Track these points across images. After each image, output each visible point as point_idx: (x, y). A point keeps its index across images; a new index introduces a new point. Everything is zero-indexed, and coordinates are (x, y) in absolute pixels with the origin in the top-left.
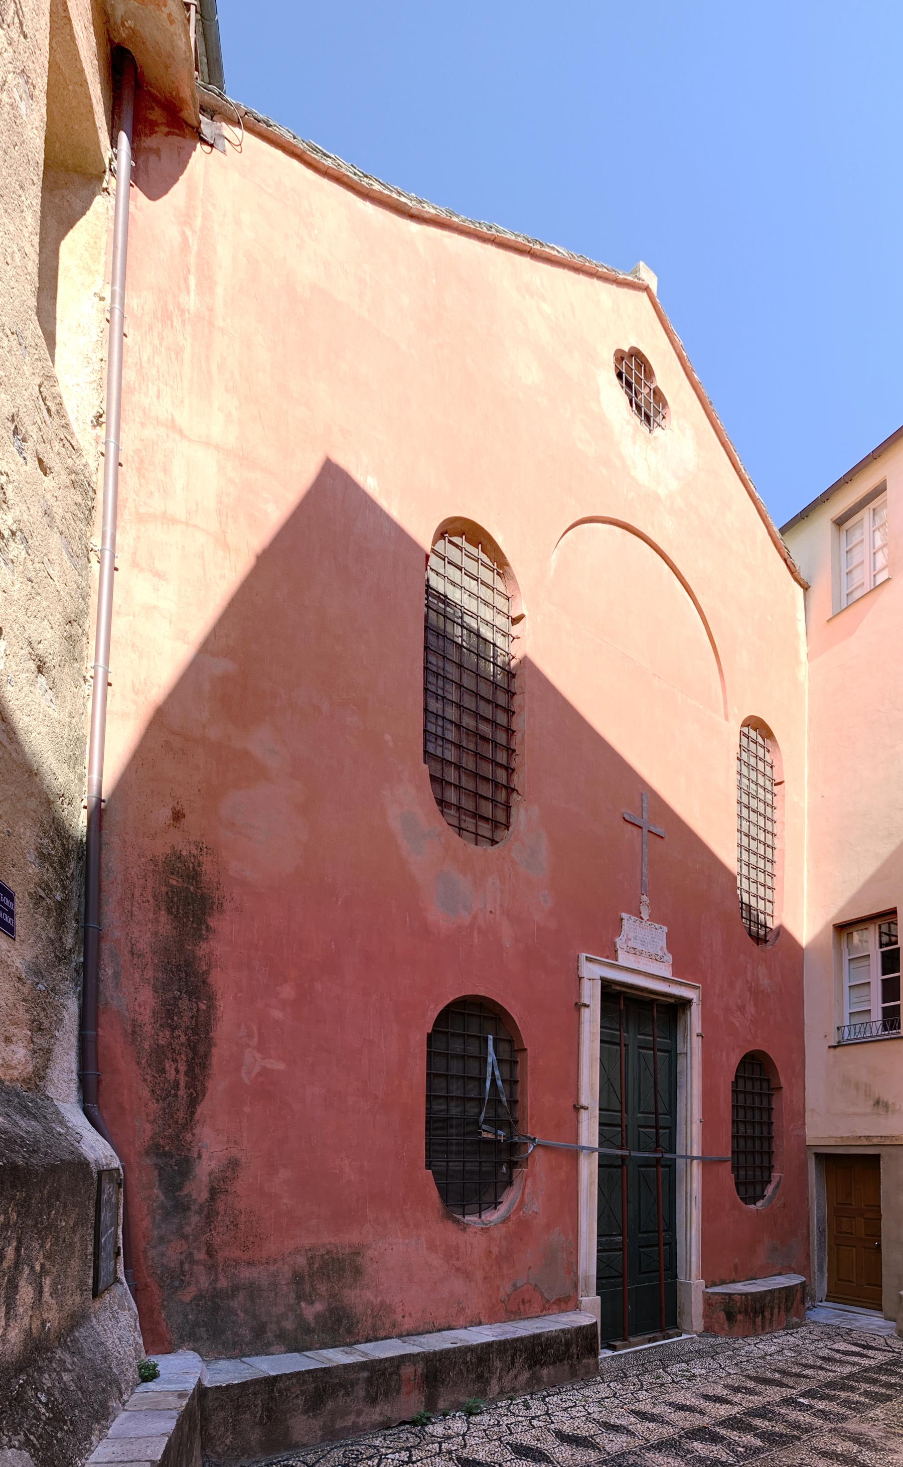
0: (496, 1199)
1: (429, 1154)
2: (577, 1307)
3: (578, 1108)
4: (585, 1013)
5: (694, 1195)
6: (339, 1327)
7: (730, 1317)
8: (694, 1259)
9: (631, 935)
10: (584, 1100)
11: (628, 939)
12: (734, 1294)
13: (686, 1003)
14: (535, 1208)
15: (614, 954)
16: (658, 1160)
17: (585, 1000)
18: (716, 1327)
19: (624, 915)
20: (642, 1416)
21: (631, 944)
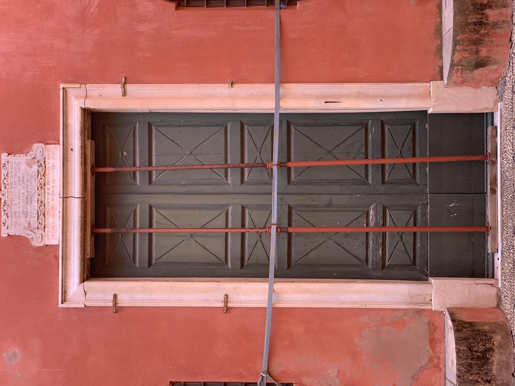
4: (124, 301)
6: (471, 234)
7: (481, 64)
9: (23, 221)
12: (452, 60)
14: (333, 373)
15: (49, 250)
16: (280, 230)
18: (493, 76)
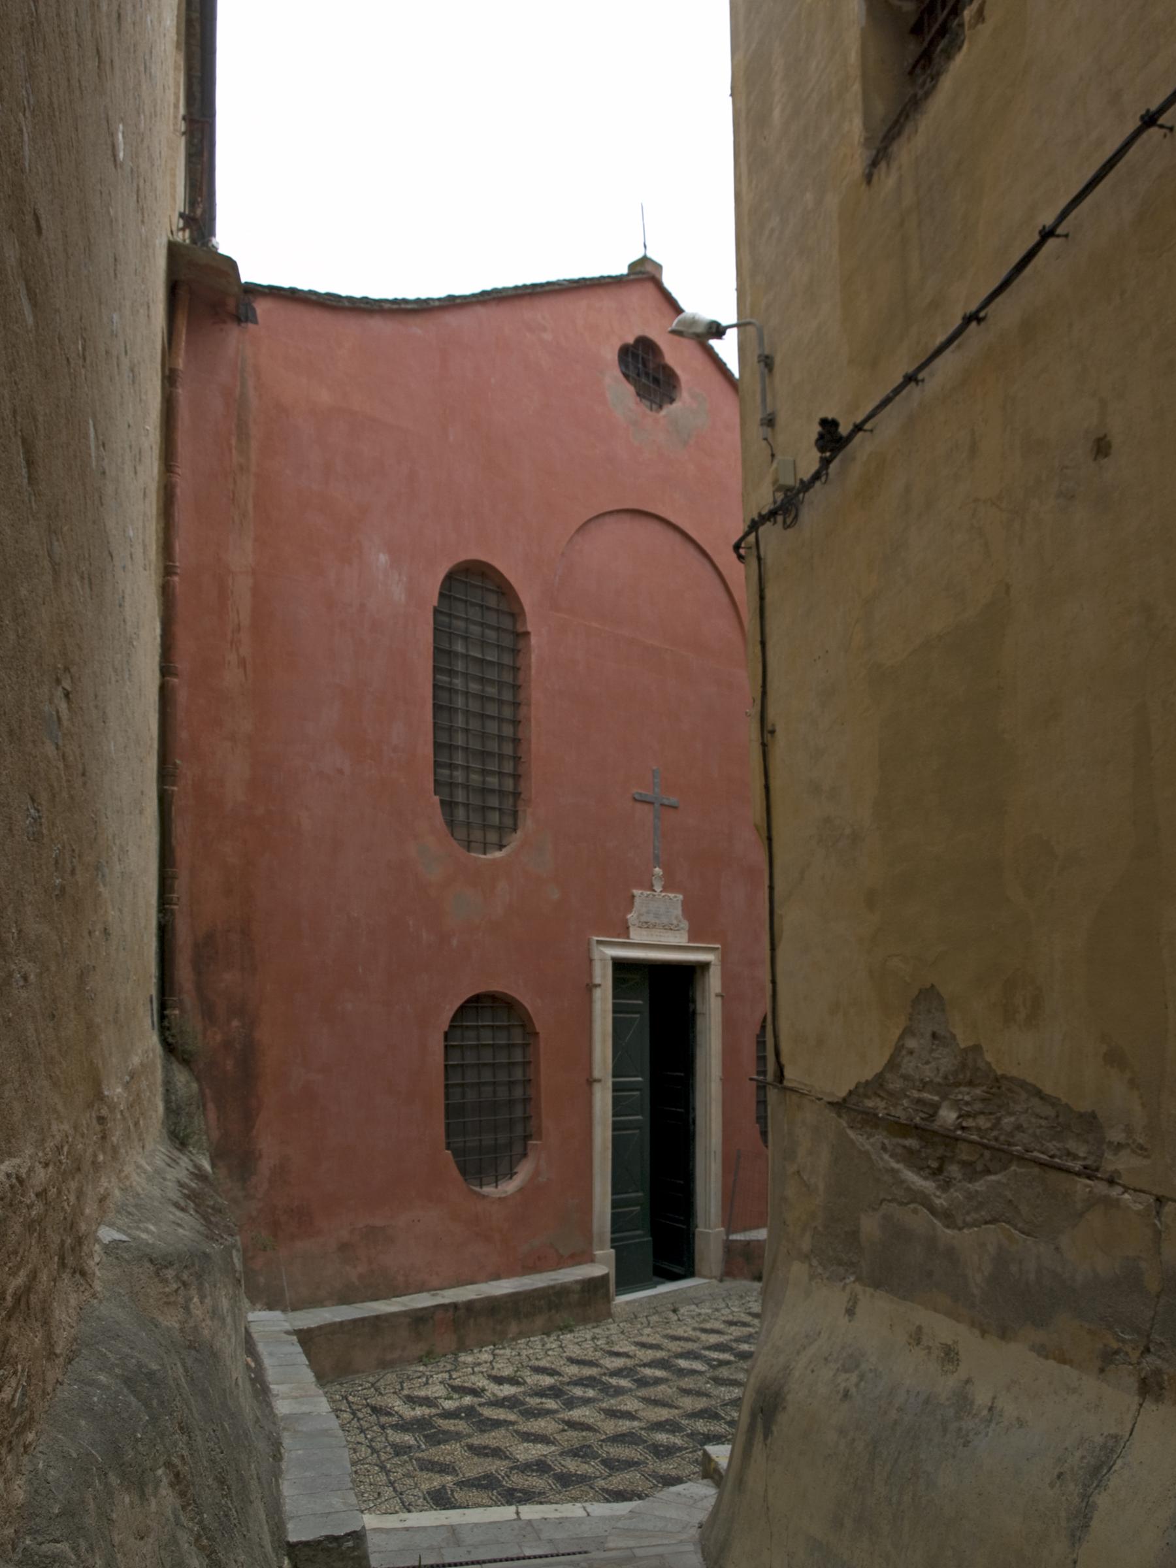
0: (511, 1169)
1: (448, 1136)
2: (592, 1260)
3: (591, 1082)
4: (597, 993)
5: (713, 1149)
8: (713, 1210)
10: (597, 1074)
11: (640, 915)
13: (705, 966)
17: (597, 980)
19: (636, 892)
20: (643, 1345)
21: (643, 919)
